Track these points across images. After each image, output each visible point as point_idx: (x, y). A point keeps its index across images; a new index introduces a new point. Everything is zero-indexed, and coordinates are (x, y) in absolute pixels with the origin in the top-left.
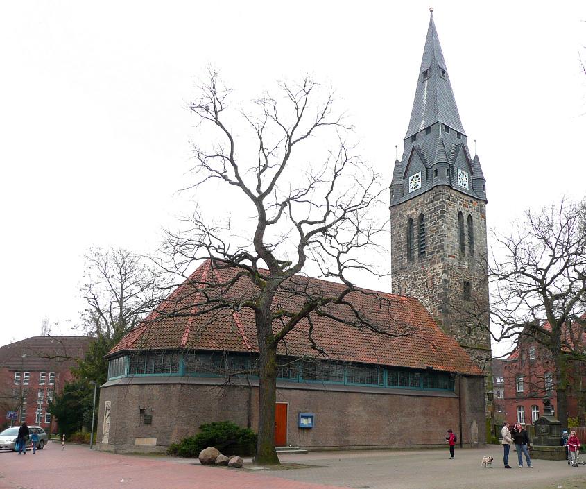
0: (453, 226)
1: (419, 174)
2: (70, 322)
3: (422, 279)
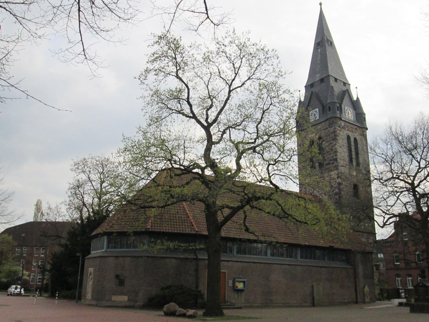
0: (343, 145)
1: (317, 110)
2: (61, 209)
3: (322, 182)
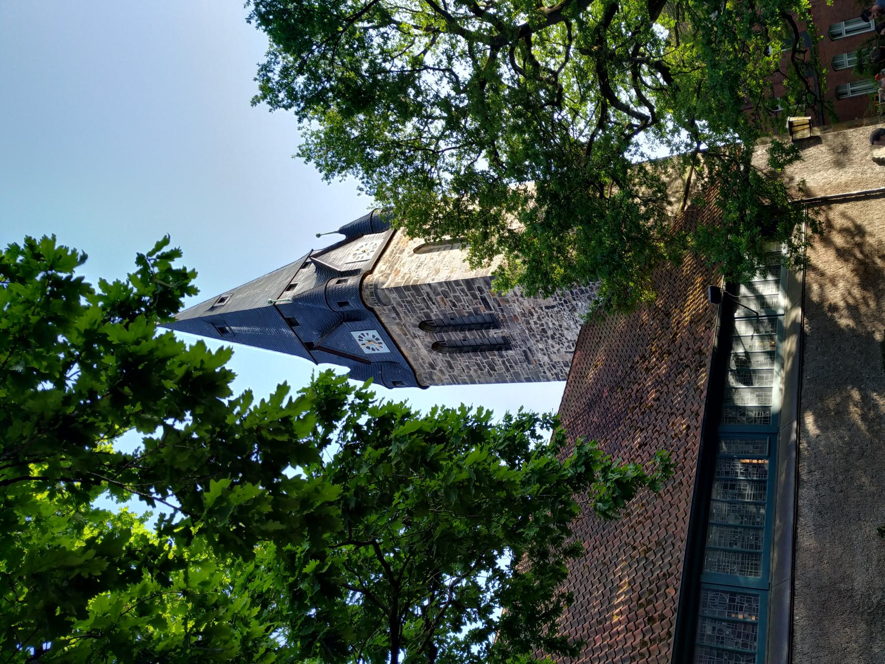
1: (356, 335)
3: (539, 318)
